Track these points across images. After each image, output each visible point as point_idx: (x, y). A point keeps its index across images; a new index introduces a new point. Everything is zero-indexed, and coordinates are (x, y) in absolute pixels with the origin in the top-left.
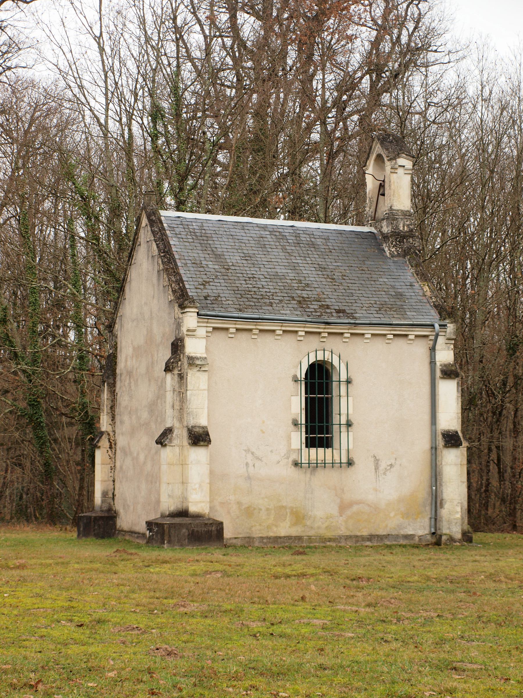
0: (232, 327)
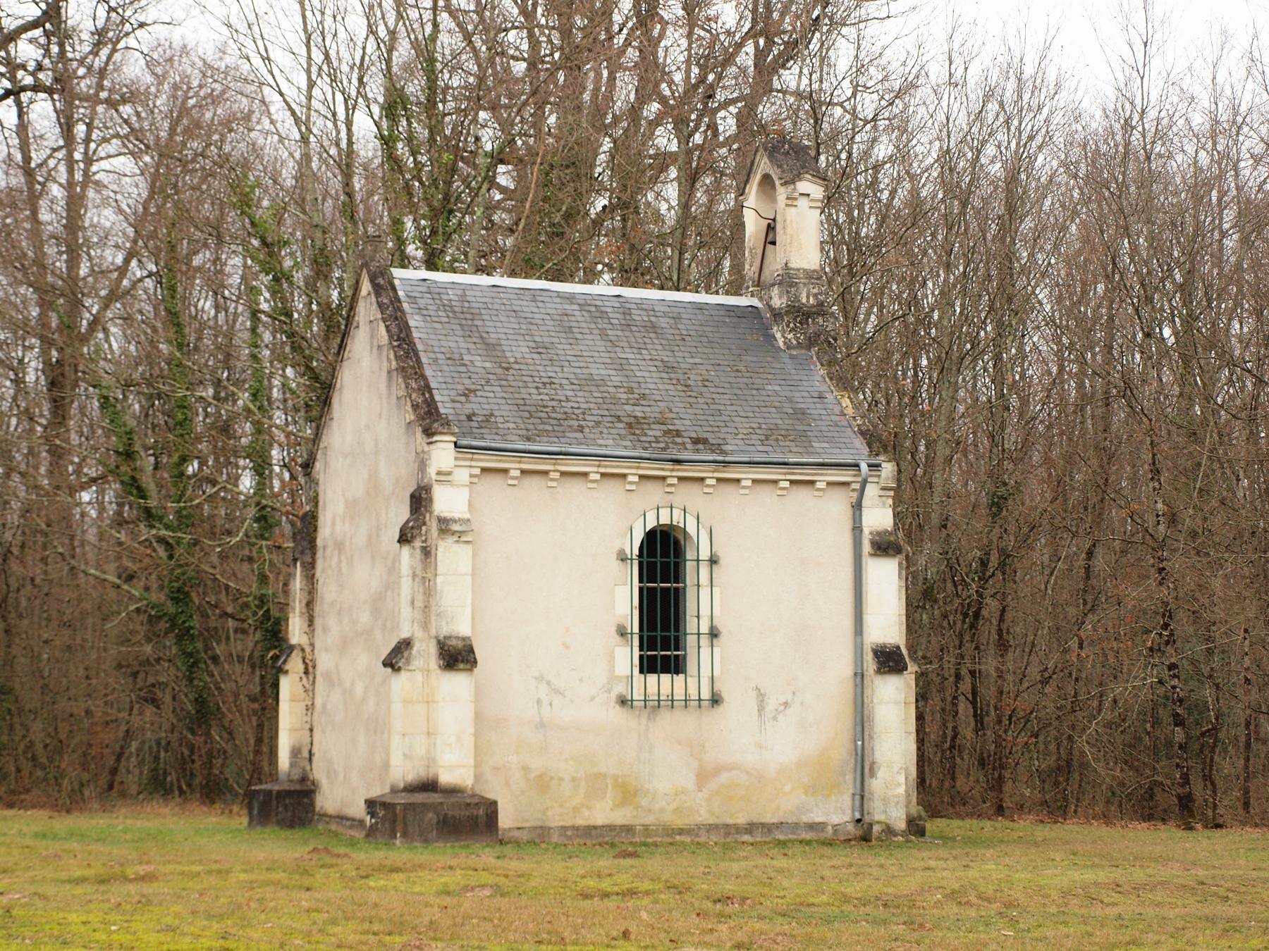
0: (514, 467)
